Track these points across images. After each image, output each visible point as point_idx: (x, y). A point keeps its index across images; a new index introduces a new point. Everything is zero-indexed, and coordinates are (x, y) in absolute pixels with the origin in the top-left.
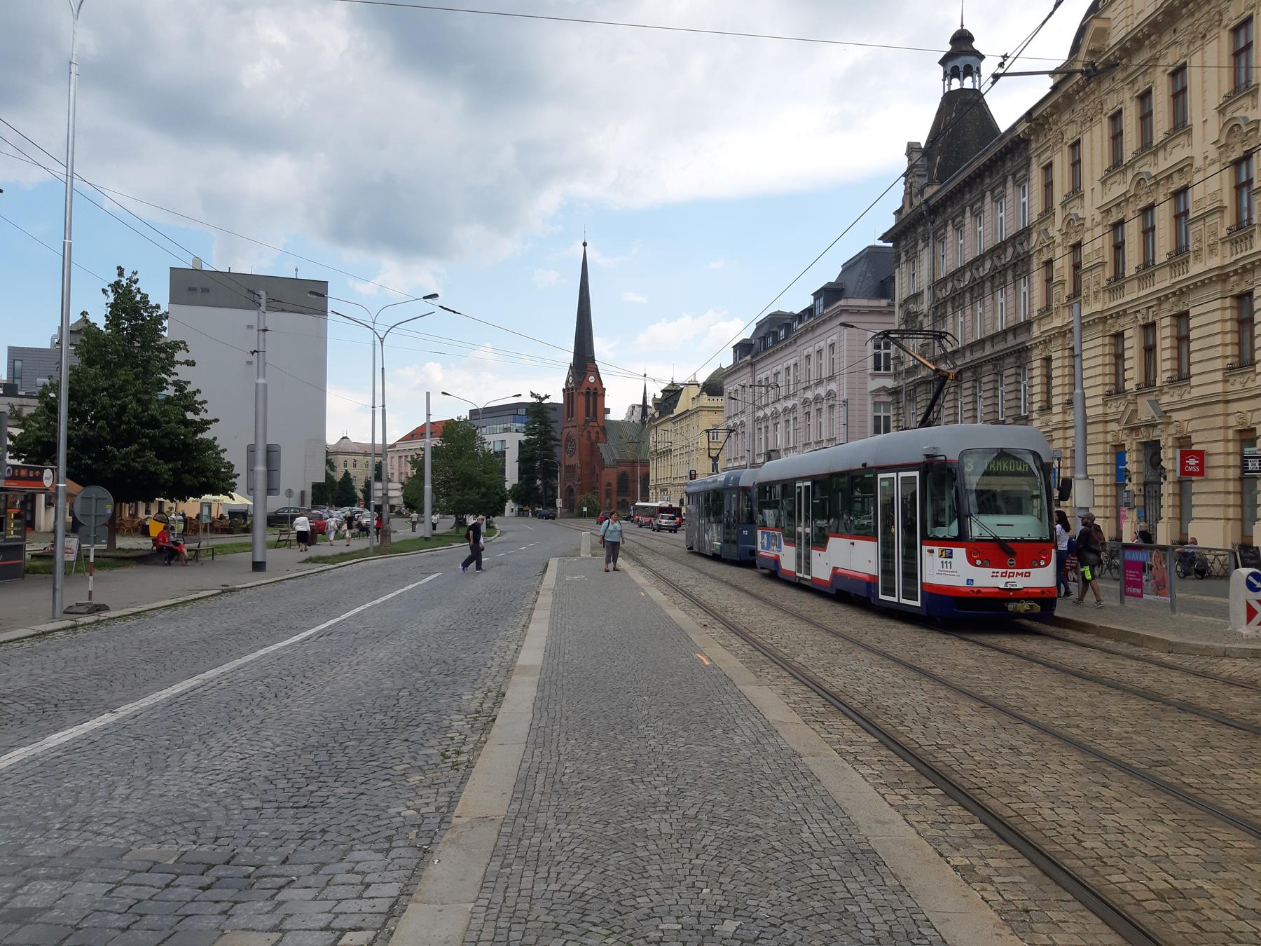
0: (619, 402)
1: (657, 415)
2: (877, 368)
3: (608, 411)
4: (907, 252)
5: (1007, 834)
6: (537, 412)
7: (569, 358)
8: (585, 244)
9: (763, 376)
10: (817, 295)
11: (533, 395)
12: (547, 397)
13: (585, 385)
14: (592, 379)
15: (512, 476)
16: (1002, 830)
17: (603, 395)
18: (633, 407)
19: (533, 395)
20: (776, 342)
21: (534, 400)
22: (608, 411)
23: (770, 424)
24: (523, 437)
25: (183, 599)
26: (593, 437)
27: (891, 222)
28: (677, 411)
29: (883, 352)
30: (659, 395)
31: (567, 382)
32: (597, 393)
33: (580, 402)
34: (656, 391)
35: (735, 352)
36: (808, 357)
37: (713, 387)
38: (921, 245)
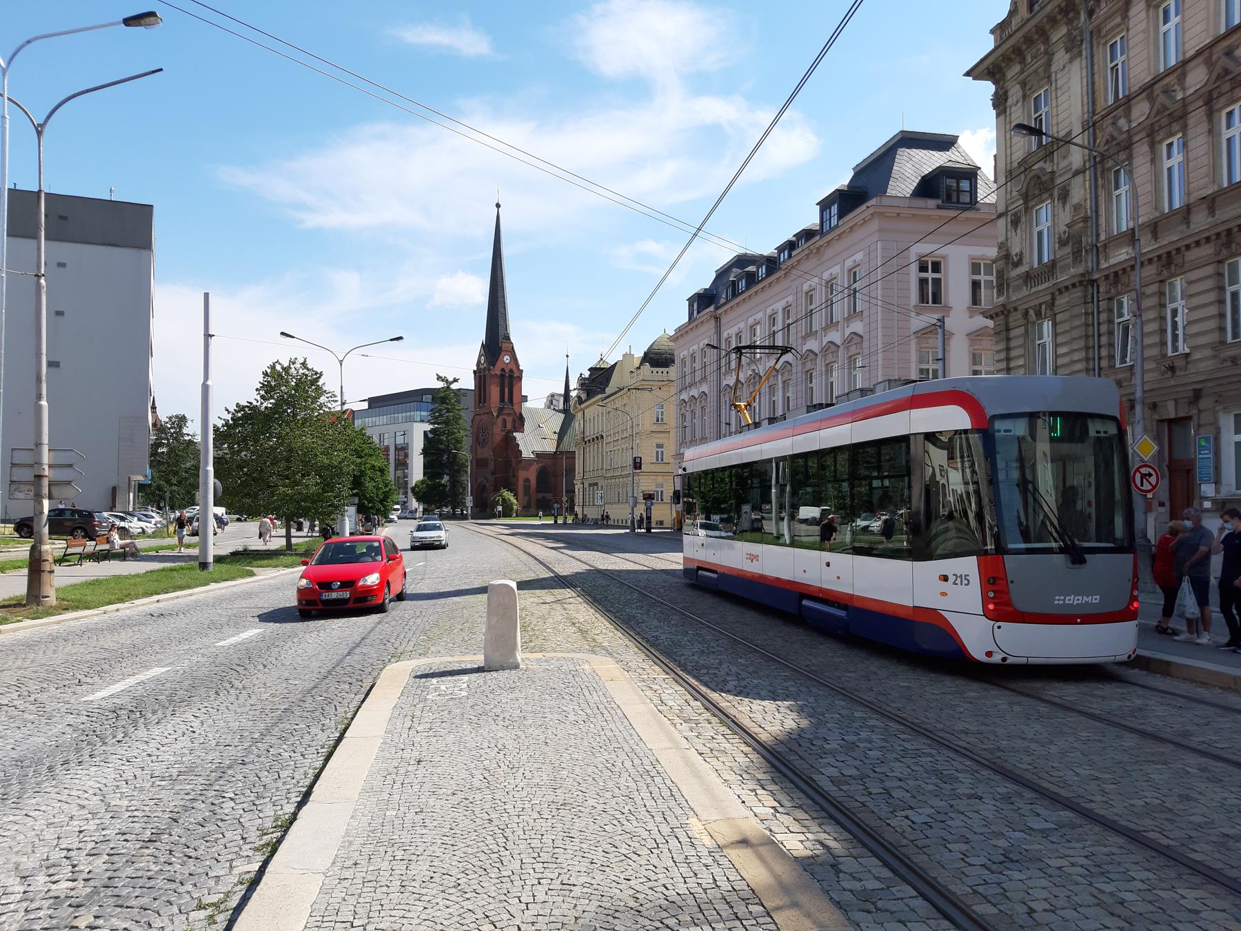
0: (539, 387)
1: (584, 396)
2: (923, 298)
3: (525, 399)
4: (1023, 84)
5: (911, 877)
6: (439, 400)
7: (482, 337)
8: (498, 206)
9: (733, 331)
10: (824, 205)
11: (439, 378)
12: (455, 380)
13: (499, 366)
14: (507, 359)
15: (417, 472)
16: (903, 870)
17: (520, 378)
18: (553, 396)
19: (439, 378)
20: (735, 294)
21: (440, 385)
22: (525, 399)
23: (820, 363)
24: (428, 427)
25: (126, 610)
26: (509, 426)
27: (987, 44)
28: (609, 391)
29: (930, 275)
30: (587, 374)
31: (479, 363)
32: (512, 378)
33: (494, 392)
34: (581, 369)
35: (691, 305)
36: (830, 285)
37: (656, 358)
38: (1061, 57)
